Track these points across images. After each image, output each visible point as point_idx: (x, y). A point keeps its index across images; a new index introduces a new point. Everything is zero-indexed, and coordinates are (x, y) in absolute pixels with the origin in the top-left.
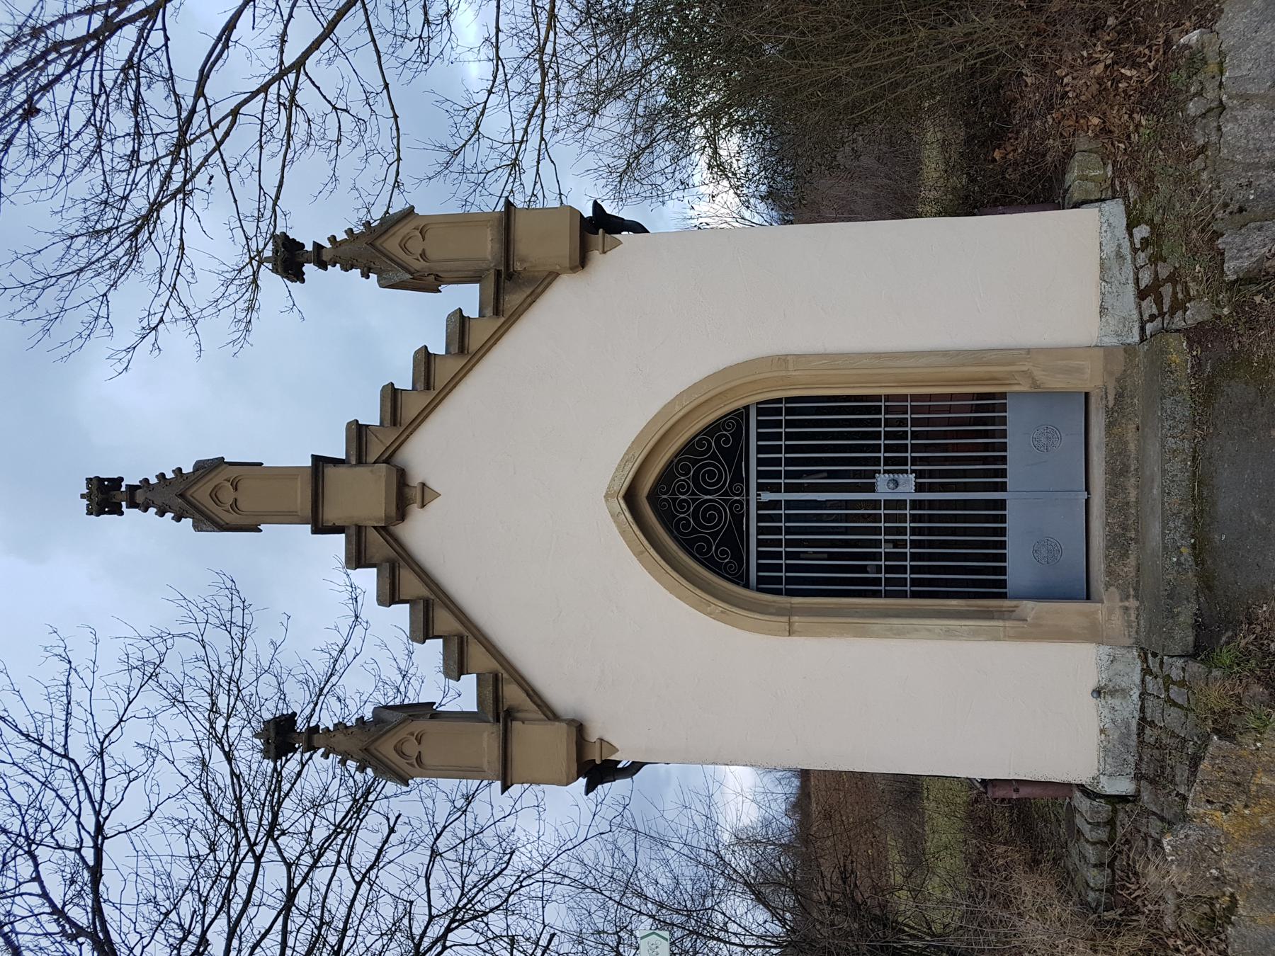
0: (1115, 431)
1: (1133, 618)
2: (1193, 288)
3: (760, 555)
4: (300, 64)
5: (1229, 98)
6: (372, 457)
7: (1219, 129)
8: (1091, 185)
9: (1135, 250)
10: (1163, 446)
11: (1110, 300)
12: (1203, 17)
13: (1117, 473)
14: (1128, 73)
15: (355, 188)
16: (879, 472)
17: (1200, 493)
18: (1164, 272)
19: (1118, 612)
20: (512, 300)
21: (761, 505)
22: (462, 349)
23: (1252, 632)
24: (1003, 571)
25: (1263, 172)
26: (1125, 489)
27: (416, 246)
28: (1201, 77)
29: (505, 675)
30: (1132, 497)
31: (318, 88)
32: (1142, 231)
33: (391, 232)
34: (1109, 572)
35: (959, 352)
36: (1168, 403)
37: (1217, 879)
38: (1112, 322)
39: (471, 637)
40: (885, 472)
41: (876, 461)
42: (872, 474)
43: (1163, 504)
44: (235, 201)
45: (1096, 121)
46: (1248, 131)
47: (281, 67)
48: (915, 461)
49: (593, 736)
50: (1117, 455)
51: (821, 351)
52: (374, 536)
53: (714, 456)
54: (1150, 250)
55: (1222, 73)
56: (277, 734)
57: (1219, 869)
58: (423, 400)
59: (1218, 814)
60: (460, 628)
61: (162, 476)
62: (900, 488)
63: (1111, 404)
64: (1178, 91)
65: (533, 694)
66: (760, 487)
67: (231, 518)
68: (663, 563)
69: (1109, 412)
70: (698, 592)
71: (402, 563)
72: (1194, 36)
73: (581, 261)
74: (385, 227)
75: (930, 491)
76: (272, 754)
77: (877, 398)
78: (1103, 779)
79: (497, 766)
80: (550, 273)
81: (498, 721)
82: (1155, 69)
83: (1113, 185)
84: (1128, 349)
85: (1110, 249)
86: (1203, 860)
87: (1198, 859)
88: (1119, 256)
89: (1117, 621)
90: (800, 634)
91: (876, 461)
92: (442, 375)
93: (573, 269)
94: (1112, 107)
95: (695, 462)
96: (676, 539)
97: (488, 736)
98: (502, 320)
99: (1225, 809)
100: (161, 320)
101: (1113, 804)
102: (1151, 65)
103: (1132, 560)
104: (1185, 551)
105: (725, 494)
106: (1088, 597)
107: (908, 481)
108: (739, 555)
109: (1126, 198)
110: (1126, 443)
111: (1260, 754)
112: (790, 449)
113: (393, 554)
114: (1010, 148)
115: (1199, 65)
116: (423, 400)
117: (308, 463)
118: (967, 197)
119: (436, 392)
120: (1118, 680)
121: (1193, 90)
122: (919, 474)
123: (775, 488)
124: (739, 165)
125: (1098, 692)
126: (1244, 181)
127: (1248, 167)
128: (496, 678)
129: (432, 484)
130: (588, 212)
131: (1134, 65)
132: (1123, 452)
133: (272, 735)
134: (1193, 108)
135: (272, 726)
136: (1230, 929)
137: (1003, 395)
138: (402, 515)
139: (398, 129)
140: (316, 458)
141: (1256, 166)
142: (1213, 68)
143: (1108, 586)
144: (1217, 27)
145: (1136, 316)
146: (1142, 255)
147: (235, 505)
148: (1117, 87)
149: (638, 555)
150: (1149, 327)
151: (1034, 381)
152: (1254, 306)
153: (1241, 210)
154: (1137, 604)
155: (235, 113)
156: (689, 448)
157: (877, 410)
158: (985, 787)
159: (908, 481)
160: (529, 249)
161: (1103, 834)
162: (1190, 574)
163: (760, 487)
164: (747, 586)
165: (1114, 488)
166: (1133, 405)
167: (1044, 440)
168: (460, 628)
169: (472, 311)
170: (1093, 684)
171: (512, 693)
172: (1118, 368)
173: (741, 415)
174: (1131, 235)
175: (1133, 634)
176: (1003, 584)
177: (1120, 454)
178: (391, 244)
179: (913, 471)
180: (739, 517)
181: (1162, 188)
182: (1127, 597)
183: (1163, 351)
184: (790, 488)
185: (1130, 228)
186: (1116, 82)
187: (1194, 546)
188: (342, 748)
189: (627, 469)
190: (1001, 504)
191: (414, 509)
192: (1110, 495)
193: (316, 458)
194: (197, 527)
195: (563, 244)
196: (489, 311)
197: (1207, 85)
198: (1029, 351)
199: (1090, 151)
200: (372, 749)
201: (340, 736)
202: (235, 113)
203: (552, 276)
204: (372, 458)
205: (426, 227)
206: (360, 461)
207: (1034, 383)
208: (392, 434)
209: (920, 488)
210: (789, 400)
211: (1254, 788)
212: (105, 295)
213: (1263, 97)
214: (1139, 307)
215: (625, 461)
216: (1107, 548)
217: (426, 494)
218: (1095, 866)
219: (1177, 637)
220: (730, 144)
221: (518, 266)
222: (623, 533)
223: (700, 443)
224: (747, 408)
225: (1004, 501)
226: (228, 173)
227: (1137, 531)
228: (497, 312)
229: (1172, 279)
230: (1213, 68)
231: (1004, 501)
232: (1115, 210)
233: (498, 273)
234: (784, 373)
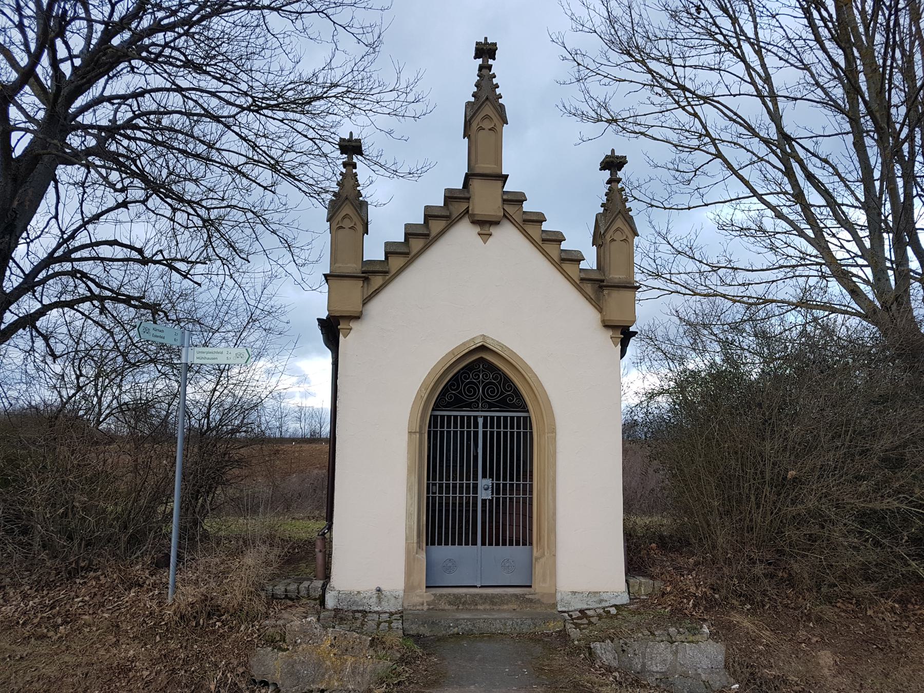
0: (513, 599)
1: (418, 608)
2: (586, 632)
3: (449, 417)
4: (719, 155)
5: (676, 646)
6: (507, 208)
7: (662, 641)
8: (637, 588)
9: (604, 608)
10: (508, 619)
11: (579, 596)
12: (715, 635)
13: (491, 599)
14: (691, 603)
15: (651, 179)
16: (493, 480)
17: (485, 636)
18: (593, 620)
19: (421, 600)
20: (588, 288)
21: (476, 418)
22: (563, 260)
23: (423, 654)
24: (440, 544)
25: (641, 660)
26: (484, 603)
27: (618, 236)
28: (687, 633)
29: (387, 277)
30: (479, 607)
31: (708, 163)
32: (613, 611)
33: (626, 223)
34: (441, 596)
35: (555, 520)
36: (529, 621)
37: (296, 642)
39: (408, 259)
40: (493, 484)
41: (498, 479)
42: (491, 476)
43: (479, 619)
44: (645, 115)
45: (668, 589)
46: (660, 654)
47: (718, 140)
48: (498, 499)
49: (353, 324)
50: (502, 599)
51: (557, 451)
52: (463, 206)
53: (502, 393)
54: (604, 614)
55: (688, 642)
56: (353, 146)
57: (300, 643)
58: (537, 237)
59: (329, 642)
60: (413, 254)
61: (497, 86)
62: (484, 491)
63: (527, 596)
64: (680, 624)
65: (377, 292)
66: (485, 418)
67: (474, 126)
68: (448, 365)
69: (523, 595)
70: (433, 384)
71: (449, 222)
72: (706, 630)
73: (607, 326)
74: (628, 219)
75: (477, 507)
76: (342, 143)
77: (531, 479)
78: (333, 593)
79: (337, 272)
80: (602, 309)
81: (363, 273)
82: (692, 615)
83: (636, 598)
84: (554, 605)
85: (605, 596)
86: (305, 636)
87: (305, 633)
88: (601, 601)
89: (417, 600)
90: (410, 438)
91: (498, 479)
92: (550, 248)
93: (603, 321)
94: (675, 596)
95: (499, 383)
96: (459, 372)
97: (353, 267)
98: (578, 282)
99: (332, 645)
100: (579, 64)
101: (319, 598)
102: (694, 613)
103: (447, 607)
104: (456, 630)
105: (482, 399)
106: (427, 587)
107: (488, 495)
108: (449, 406)
109: (630, 604)
110: (507, 604)
111: (365, 658)
112: (512, 434)
113: (454, 216)
114: (657, 551)
115: (692, 632)
116: (537, 237)
117: (504, 173)
119: (540, 243)
121: (681, 630)
122: (491, 501)
123: (485, 426)
124: (653, 405)
125: (379, 590)
126: (637, 652)
127: (644, 655)
128: (386, 272)
129: (491, 239)
130: (631, 329)
131: (694, 606)
132: (502, 603)
133: (354, 144)
134: (672, 630)
135: (358, 144)
136: (270, 649)
137: (531, 544)
138: (474, 222)
139: (682, 209)
140: (506, 177)
141: (644, 657)
142: (691, 638)
143: (435, 595)
144: (710, 640)
145: (571, 609)
146: (602, 611)
148: (684, 598)
149: (452, 352)
150: (566, 615)
151: (539, 558)
152: (579, 654)
153: (623, 651)
154: (425, 609)
155: (695, 115)
156: (507, 380)
157: (525, 479)
158: (322, 535)
159: (488, 495)
160: (614, 298)
161: (303, 592)
162: (444, 632)
163: (485, 418)
164: (433, 410)
165: (485, 599)
166: (526, 607)
167: (507, 565)
168: (413, 254)
169: (583, 265)
170: (383, 587)
171: (377, 281)
172: (545, 600)
173: (525, 408)
174: (611, 606)
175: (410, 608)
176: (433, 544)
177: (502, 601)
178: (619, 223)
179: (493, 498)
180: (470, 406)
181: (635, 618)
182: (428, 605)
183: (555, 619)
184: (485, 433)
185: (615, 606)
186: (685, 597)
187: (458, 634)
188: (346, 184)
189: (498, 347)
191: (477, 229)
192: (481, 596)
193: (506, 177)
194: (468, 104)
195: (617, 317)
196: (583, 275)
197: (683, 636)
198: (555, 555)
199: (654, 588)
200: (347, 201)
201: (352, 182)
202: (695, 115)
203: (600, 310)
204: (506, 207)
205: (628, 242)
206: (504, 201)
207: (537, 559)
208: (519, 220)
209: (484, 501)
210: (531, 433)
211: (345, 657)
212: (595, 32)
213: (676, 660)
214: (576, 610)
215: (503, 346)
216: (454, 594)
217: (485, 236)
218: (286, 589)
219: (412, 626)
220: (663, 401)
221: (606, 292)
222: (464, 344)
223: (509, 386)
224: (528, 411)
225: (476, 545)
226: (661, 112)
227: (462, 609)
228: (582, 280)
229: (590, 623)
230: (691, 638)
231: (476, 545)
232: (624, 599)
233: (602, 281)
234: (546, 431)
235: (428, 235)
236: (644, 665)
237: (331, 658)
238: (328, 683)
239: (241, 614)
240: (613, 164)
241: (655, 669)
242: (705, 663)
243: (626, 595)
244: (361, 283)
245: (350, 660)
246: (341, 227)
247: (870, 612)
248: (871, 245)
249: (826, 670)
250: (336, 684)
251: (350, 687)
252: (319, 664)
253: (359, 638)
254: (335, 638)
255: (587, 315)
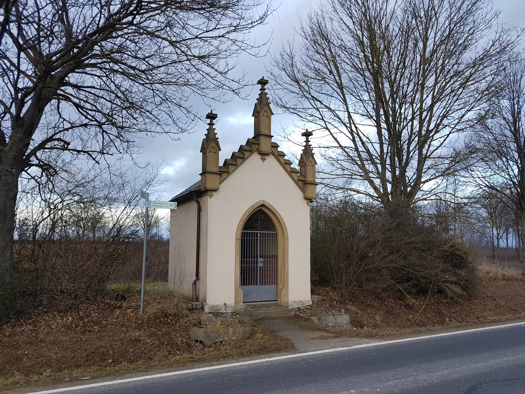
11: (296, 303)
20: (300, 183)
22: (292, 172)
26: (264, 307)
30: (262, 309)
34: (249, 305)
36: (284, 312)
38: (292, 303)
49: (213, 193)
50: (271, 306)
52: (257, 147)
53: (267, 224)
73: (306, 198)
85: (304, 302)
87: (209, 320)
88: (303, 304)
89: (240, 307)
95: (266, 219)
99: (221, 324)
118: (165, 315)
120: (228, 308)
122: (262, 267)
125: (225, 304)
129: (265, 161)
132: (270, 307)
142: (339, 314)
147: (264, 115)
160: (309, 188)
172: (285, 305)
180: (256, 229)
184: (260, 239)
190: (257, 284)
191: (260, 157)
192: (263, 304)
203: (304, 191)
209: (260, 267)
215: (270, 205)
217: (263, 160)
221: (307, 185)
222: (256, 203)
223: (269, 221)
230: (339, 314)
232: (311, 303)
233: (305, 181)
235: (244, 158)
236: (326, 324)
237: (222, 329)
238: (223, 339)
239: (177, 316)
240: (307, 134)
241: (330, 325)
242: (345, 322)
243: (311, 301)
244: (219, 176)
245: (231, 329)
246: (211, 152)
247: (386, 303)
248: (54, 56)
249: (378, 322)
250: (226, 338)
251: (234, 339)
252: (218, 332)
253: (234, 320)
254: (222, 322)
255: (299, 194)
